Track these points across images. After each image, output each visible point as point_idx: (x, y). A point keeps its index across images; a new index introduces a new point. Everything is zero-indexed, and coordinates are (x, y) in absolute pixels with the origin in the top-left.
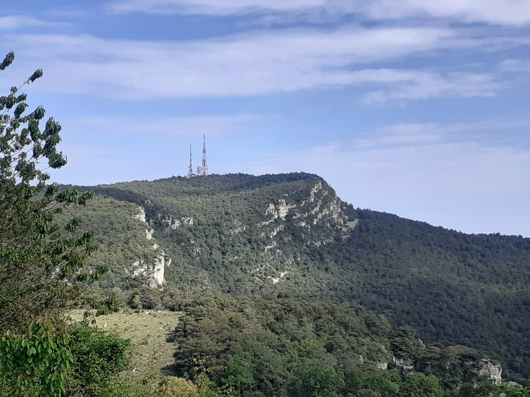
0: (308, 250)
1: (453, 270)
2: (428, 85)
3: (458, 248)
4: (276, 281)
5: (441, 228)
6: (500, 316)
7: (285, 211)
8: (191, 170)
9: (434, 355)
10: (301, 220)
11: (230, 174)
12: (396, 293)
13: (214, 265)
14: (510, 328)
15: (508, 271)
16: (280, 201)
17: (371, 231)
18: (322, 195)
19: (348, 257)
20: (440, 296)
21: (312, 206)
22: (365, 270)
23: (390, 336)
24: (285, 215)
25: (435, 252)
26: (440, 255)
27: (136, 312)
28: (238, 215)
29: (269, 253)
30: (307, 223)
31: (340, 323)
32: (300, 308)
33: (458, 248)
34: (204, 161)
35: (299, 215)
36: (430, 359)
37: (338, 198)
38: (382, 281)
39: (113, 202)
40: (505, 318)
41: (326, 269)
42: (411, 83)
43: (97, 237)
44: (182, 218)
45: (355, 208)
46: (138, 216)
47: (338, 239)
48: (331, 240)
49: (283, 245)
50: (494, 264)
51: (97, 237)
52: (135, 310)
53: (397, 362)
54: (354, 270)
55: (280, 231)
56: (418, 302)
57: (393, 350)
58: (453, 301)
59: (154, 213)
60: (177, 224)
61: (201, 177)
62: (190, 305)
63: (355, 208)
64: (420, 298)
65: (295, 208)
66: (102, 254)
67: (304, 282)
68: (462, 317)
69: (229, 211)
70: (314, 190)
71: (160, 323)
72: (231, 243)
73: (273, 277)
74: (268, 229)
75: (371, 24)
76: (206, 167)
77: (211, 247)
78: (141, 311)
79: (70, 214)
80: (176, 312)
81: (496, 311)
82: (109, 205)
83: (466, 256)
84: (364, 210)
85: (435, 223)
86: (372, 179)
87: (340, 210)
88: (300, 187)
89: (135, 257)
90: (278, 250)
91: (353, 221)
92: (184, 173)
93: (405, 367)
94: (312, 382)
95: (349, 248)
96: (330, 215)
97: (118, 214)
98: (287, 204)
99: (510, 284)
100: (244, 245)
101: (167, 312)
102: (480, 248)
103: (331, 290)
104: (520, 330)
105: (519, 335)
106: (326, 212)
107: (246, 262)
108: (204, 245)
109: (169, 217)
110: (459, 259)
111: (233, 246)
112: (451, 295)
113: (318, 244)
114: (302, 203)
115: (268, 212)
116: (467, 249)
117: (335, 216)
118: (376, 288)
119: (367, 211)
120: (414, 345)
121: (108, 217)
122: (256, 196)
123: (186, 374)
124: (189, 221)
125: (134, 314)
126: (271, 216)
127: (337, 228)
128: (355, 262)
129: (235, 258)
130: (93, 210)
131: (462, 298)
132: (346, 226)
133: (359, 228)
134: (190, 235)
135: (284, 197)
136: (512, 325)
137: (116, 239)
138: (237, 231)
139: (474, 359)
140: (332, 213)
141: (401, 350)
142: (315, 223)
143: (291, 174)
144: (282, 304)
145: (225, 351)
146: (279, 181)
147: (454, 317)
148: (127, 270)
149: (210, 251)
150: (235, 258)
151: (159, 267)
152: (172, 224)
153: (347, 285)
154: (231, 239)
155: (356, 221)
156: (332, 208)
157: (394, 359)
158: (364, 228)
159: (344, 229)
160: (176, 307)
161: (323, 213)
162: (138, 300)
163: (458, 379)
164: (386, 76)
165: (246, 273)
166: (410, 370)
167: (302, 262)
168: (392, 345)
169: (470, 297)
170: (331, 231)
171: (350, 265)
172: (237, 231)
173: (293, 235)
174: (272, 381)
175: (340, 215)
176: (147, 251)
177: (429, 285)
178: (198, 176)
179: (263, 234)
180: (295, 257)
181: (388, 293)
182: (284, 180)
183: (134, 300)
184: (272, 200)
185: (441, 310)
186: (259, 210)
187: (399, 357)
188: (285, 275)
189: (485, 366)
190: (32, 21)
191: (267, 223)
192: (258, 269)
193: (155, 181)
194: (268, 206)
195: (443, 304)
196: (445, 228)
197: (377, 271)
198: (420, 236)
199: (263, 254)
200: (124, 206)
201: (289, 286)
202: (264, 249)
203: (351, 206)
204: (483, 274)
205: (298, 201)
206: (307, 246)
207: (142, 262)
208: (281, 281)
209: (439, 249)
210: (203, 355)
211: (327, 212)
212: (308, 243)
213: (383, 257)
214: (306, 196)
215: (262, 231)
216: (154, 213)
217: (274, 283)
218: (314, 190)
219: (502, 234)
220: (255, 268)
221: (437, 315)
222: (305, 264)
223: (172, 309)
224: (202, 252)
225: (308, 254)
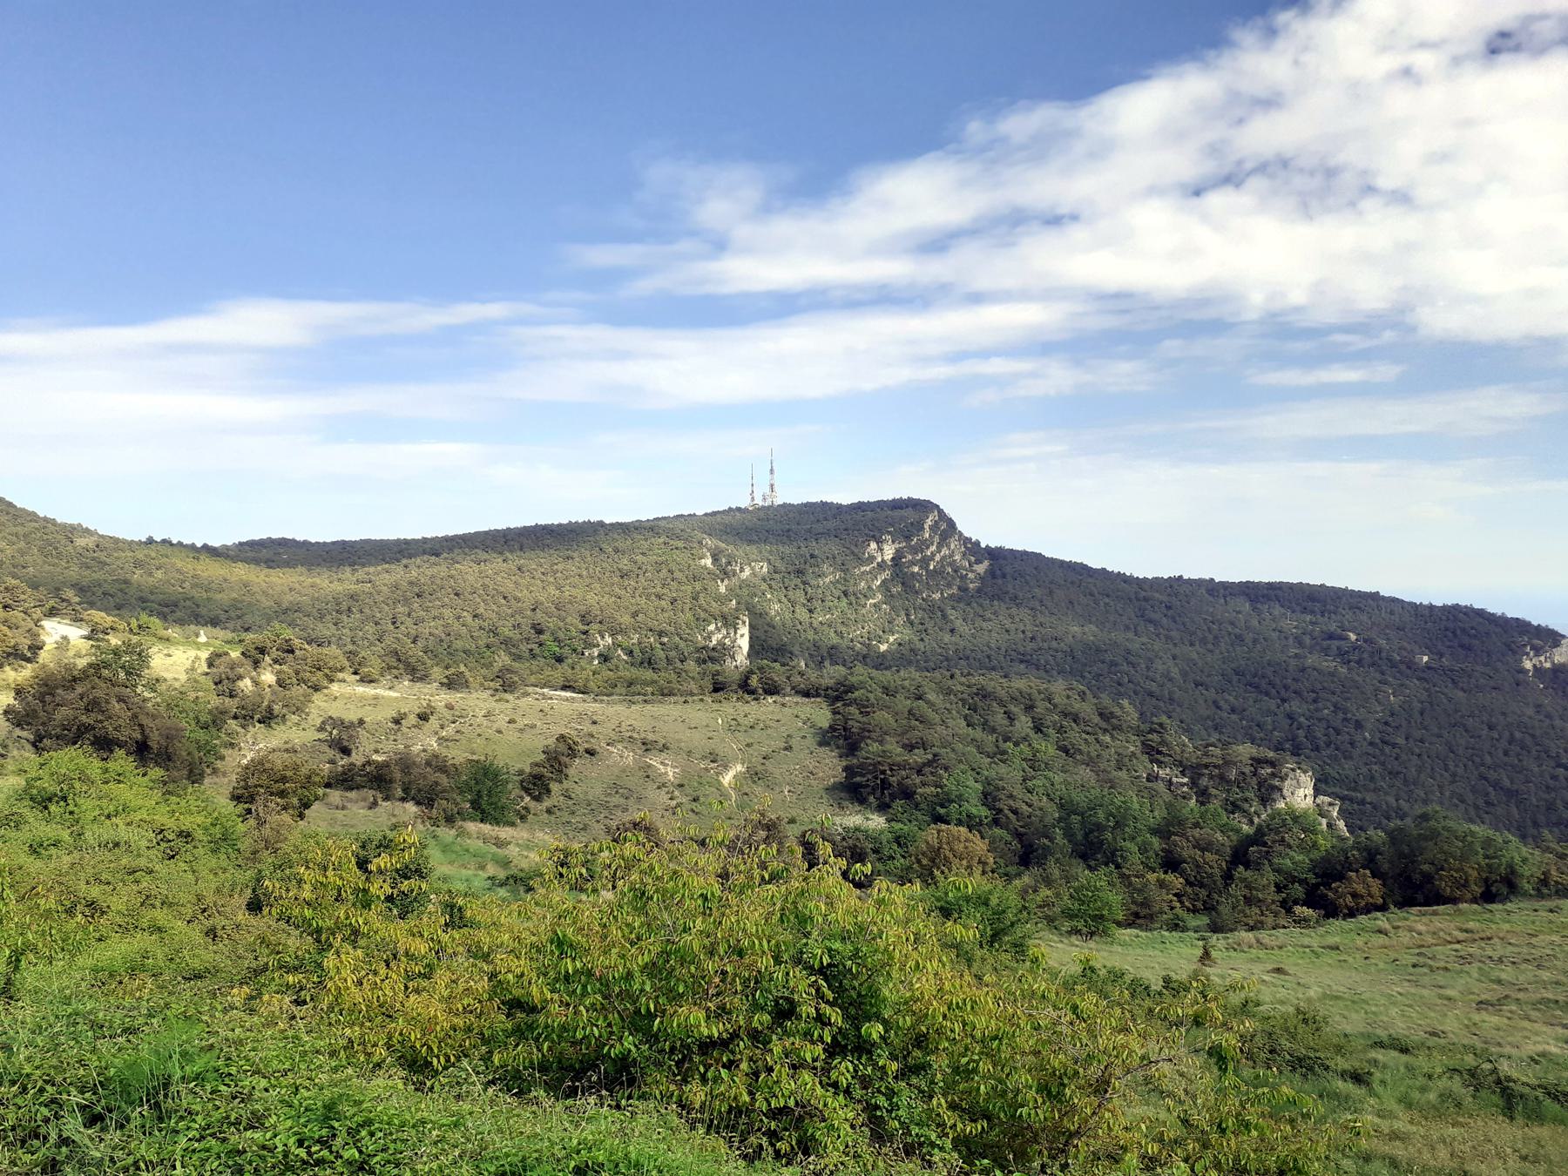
1: (1127, 628)
2: (1059, 377)
4: (883, 647)
9: (1214, 760)
10: (913, 563)
14: (1218, 708)
21: (926, 544)
30: (921, 568)
32: (1002, 693)
36: (1206, 766)
38: (1032, 645)
40: (1211, 694)
41: (952, 631)
42: (1033, 375)
48: (954, 590)
68: (1151, 694)
70: (929, 522)
75: (977, 298)
86: (1014, 503)
88: (909, 518)
93: (1175, 780)
94: (1101, 815)
96: (951, 556)
99: (1210, 646)
101: (798, 699)
102: (1164, 598)
104: (1233, 710)
105: (1234, 717)
106: (945, 551)
113: (937, 596)
116: (1146, 599)
117: (957, 557)
121: (665, 563)
123: (872, 799)
126: (872, 558)
131: (1148, 668)
133: (991, 573)
134: (764, 586)
136: (1222, 703)
139: (1272, 764)
141: (1159, 752)
145: (929, 763)
155: (986, 563)
159: (971, 575)
163: (1251, 795)
164: (997, 366)
166: (1183, 785)
168: (1143, 743)
169: (1159, 666)
174: (1015, 812)
177: (1098, 650)
178: (763, 507)
187: (1160, 764)
189: (1291, 775)
190: (527, 308)
203: (978, 543)
205: (908, 538)
215: (861, 579)
218: (929, 522)
223: (807, 694)
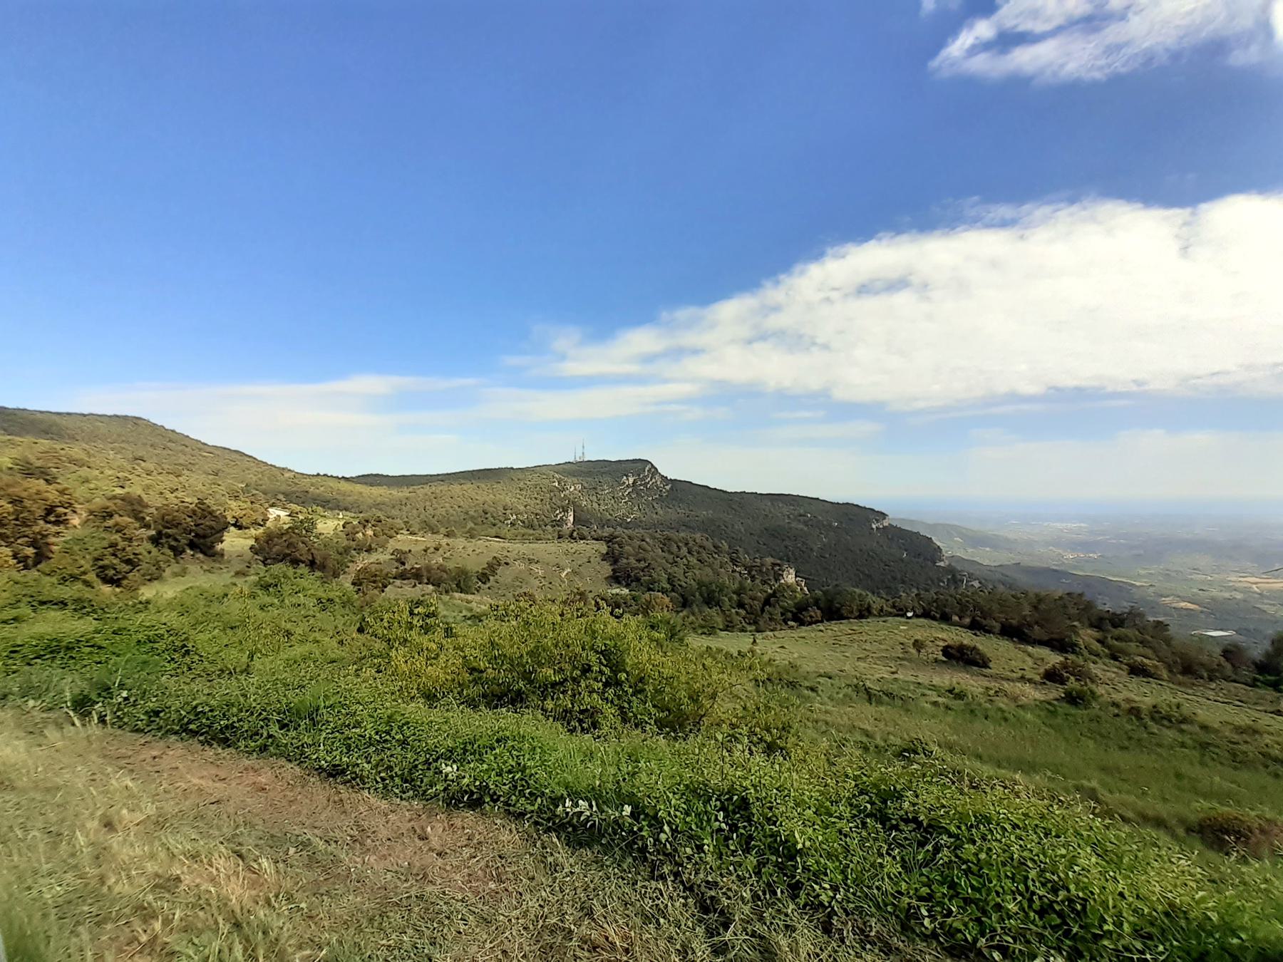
75: (666, 381)
86: (680, 462)
88: (641, 467)
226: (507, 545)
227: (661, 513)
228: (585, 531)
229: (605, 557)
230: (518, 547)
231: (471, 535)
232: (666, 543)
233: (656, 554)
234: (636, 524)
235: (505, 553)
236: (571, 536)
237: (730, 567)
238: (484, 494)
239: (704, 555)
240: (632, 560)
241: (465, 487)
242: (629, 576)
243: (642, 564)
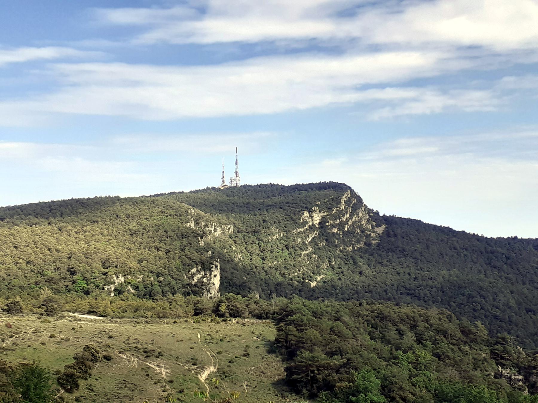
0: (341, 255)
2: (432, 101)
3: (483, 250)
4: (313, 284)
5: (464, 232)
6: (533, 316)
7: (318, 218)
8: (223, 182)
10: (333, 226)
11: (261, 184)
12: (429, 295)
13: (255, 270)
15: (533, 272)
16: (313, 208)
17: (399, 237)
18: (351, 203)
19: (381, 261)
20: (473, 297)
21: (342, 213)
22: (398, 273)
23: (488, 344)
24: (318, 221)
25: (462, 255)
26: (466, 258)
27: (224, 321)
28: (275, 222)
29: (306, 258)
31: (438, 331)
32: (395, 316)
33: (483, 250)
34: (237, 173)
35: (332, 222)
37: (365, 205)
39: (164, 212)
41: (360, 273)
42: (414, 100)
43: (154, 244)
44: (223, 226)
45: (381, 214)
46: (189, 224)
47: (368, 244)
48: (362, 245)
49: (318, 250)
50: (520, 267)
51: (154, 244)
52: (222, 319)
53: (504, 372)
54: (386, 273)
55: (315, 237)
56: (453, 304)
57: (494, 358)
58: (486, 302)
59: (198, 221)
60: (219, 232)
61: (234, 187)
62: (277, 313)
63: (381, 214)
64: (454, 300)
65: (328, 215)
66: (162, 261)
67: (340, 285)
68: (496, 317)
69: (267, 219)
70: (344, 198)
71: (253, 333)
72: (270, 249)
73: (310, 280)
74: (303, 235)
75: (376, 48)
76: (238, 178)
77: (251, 254)
78: (229, 319)
79: (124, 223)
80: (264, 321)
81: (528, 311)
82: (160, 214)
83: (491, 259)
84: (390, 216)
85: (457, 228)
86: (402, 188)
87: (367, 217)
88: (332, 195)
89: (193, 264)
90: (314, 255)
91: (380, 227)
92: (217, 184)
93: (513, 377)
95: (380, 252)
96: (359, 221)
97: (171, 223)
98: (320, 212)
100: (282, 250)
101: (254, 320)
102: (504, 251)
103: (366, 292)
106: (355, 218)
107: (285, 267)
108: (244, 251)
109: (212, 225)
110: (485, 261)
111: (271, 252)
112: (483, 296)
113: (350, 249)
114: (333, 210)
115: (303, 219)
117: (364, 222)
118: (409, 290)
119: (393, 218)
120: (515, 353)
122: (290, 205)
123: (305, 391)
124: (229, 228)
125: (222, 323)
127: (367, 234)
128: (387, 266)
129: (274, 263)
130: (146, 219)
131: (494, 300)
132: (374, 232)
133: (387, 233)
134: (231, 242)
135: (317, 205)
137: (173, 247)
138: (274, 238)
140: (361, 219)
141: (503, 358)
142: (346, 229)
143: (320, 183)
144: (372, 312)
145: (344, 365)
146: (310, 190)
147: (489, 318)
148: (185, 277)
149: (250, 257)
150: (274, 263)
151: (216, 273)
152: (215, 232)
153: (381, 287)
154: (269, 245)
155: (383, 226)
156: (360, 215)
157: (500, 369)
158: (392, 233)
159: (373, 235)
160: (264, 315)
161: (353, 220)
162: (224, 308)
164: (390, 94)
165: (285, 277)
167: (336, 266)
168: (491, 351)
169: (501, 297)
170: (361, 237)
171: (382, 269)
172: (274, 238)
173: (326, 240)
175: (368, 221)
176: (203, 258)
177: (460, 287)
179: (299, 240)
180: (329, 262)
181: (422, 295)
182: (314, 189)
183: (220, 308)
184: (306, 208)
185: (475, 310)
186: (294, 217)
187: (503, 366)
188: (321, 279)
191: (303, 230)
192: (296, 274)
193: (191, 192)
194: (303, 214)
195: (477, 305)
196: (468, 232)
197: (409, 274)
198: (446, 239)
199: (300, 259)
200: (176, 215)
201: (326, 289)
202: (301, 254)
203: (377, 213)
204: (510, 276)
205: (330, 209)
206: (341, 251)
207: (199, 268)
208: (318, 285)
209: (466, 253)
210: (320, 370)
211: (357, 219)
212: (341, 248)
213: (413, 260)
214: (337, 204)
216: (198, 221)
217: (312, 287)
218: (344, 198)
219: (519, 237)
220: (294, 273)
221: (472, 315)
222: (340, 268)
224: (243, 258)
225: (341, 258)
226: (109, 326)
227: (368, 273)
228: (239, 301)
229: (273, 348)
230: (126, 329)
231: (49, 310)
232: (377, 324)
233: (360, 341)
234: (327, 291)
235: (105, 340)
236: (216, 311)
237: (492, 368)
238: (67, 242)
239: (445, 346)
240: (320, 354)
241: (38, 230)
242: (314, 380)
243: (337, 361)
